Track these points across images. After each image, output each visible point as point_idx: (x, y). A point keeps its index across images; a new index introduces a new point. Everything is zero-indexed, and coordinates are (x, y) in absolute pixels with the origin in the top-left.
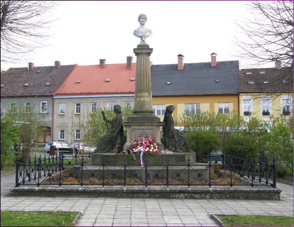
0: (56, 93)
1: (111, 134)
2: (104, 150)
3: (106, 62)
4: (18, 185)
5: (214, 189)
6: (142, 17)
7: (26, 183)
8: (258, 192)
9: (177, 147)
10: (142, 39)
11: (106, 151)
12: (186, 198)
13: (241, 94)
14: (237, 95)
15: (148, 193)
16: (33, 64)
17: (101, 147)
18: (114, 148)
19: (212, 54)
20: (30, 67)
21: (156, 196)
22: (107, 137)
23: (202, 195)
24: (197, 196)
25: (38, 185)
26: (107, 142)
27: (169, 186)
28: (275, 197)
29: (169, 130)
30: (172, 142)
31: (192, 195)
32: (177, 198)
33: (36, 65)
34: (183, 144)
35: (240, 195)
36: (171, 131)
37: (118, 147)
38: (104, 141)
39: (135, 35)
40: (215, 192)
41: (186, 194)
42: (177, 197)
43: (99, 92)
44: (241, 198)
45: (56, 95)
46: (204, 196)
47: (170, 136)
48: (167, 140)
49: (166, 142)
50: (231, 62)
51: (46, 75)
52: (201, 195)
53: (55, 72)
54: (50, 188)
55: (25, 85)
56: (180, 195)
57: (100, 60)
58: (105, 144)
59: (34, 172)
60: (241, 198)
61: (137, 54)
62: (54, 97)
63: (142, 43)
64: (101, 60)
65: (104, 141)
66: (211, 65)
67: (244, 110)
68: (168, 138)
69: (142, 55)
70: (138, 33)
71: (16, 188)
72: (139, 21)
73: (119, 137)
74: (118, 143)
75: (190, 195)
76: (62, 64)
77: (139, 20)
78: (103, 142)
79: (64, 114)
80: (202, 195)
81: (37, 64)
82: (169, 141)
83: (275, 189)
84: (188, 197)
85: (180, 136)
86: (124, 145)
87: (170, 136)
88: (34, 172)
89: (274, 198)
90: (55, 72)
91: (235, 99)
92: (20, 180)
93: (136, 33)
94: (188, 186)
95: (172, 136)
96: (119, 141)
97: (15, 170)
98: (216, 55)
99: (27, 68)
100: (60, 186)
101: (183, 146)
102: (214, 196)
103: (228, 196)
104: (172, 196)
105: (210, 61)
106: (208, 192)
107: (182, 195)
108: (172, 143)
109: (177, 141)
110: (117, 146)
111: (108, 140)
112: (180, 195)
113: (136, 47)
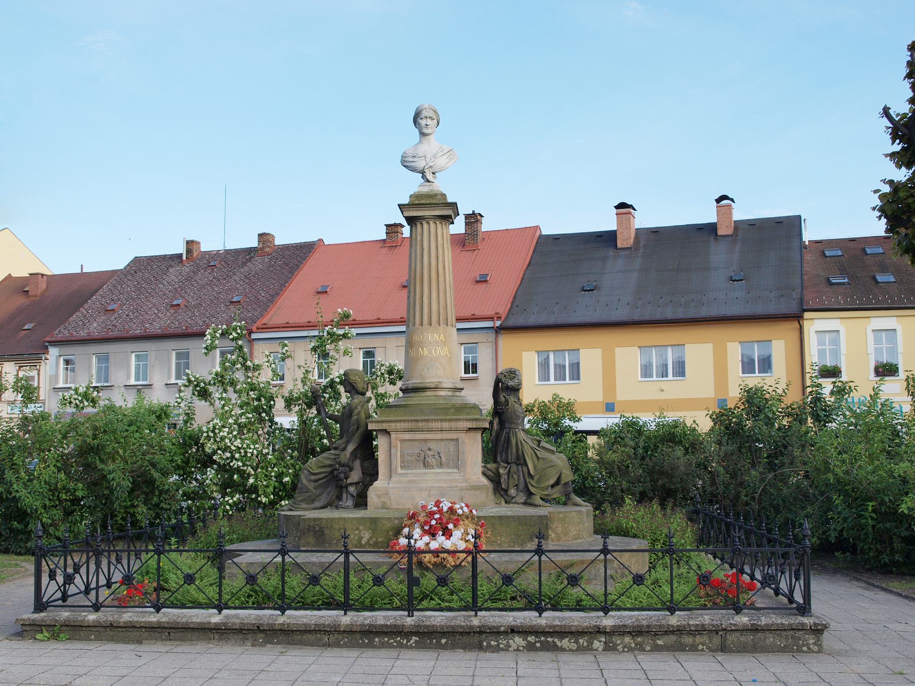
0: (259, 323)
1: (335, 455)
2: (313, 501)
3: (484, 220)
4: (40, 605)
5: (619, 622)
6: (424, 114)
7: (70, 601)
8: (755, 629)
9: (532, 490)
10: (424, 177)
11: (318, 504)
12: (531, 647)
13: (807, 315)
14: (797, 317)
15: (416, 633)
16: (198, 243)
17: (308, 492)
18: (344, 495)
19: (718, 201)
20: (189, 251)
21: (439, 642)
22: (320, 465)
23: (581, 641)
24: (565, 643)
25: (96, 607)
26: (325, 477)
27: (479, 613)
28: (808, 645)
29: (508, 440)
30: (519, 476)
31: (550, 639)
32: (502, 650)
33: (206, 246)
34: (552, 481)
35: (698, 639)
36: (514, 442)
37: (355, 494)
38: (314, 474)
39: (404, 166)
40: (619, 631)
41: (531, 639)
42: (501, 646)
43: (384, 316)
44: (700, 647)
45: (262, 329)
46: (585, 644)
47: (512, 457)
48: (501, 471)
49: (498, 475)
50: (778, 222)
51: (234, 274)
52: (577, 642)
53: (258, 264)
54: (128, 616)
55: (175, 303)
56: (511, 641)
57: (387, 225)
58: (317, 484)
59: (125, 562)
60: (700, 647)
61: (411, 220)
62: (254, 336)
63: (425, 189)
64: (387, 226)
65: (314, 474)
66: (716, 230)
67: (878, 351)
68: (506, 465)
69: (424, 223)
70: (411, 159)
71: (36, 616)
72: (415, 125)
73: (357, 464)
74: (355, 481)
75: (543, 638)
76: (280, 240)
77: (415, 121)
78: (313, 477)
79: (282, 382)
80: (581, 641)
81: (210, 244)
82: (509, 472)
83: (806, 620)
84: (538, 645)
85: (543, 459)
86: (371, 489)
87: (512, 457)
88: (125, 562)
89: (805, 649)
90: (258, 264)
91: (788, 329)
92: (51, 590)
93: (406, 164)
94: (537, 614)
95: (518, 458)
96: (356, 475)
97: (31, 568)
98: (732, 200)
99: (180, 256)
100: (158, 612)
101: (552, 486)
102: (619, 642)
103: (660, 642)
104: (489, 644)
105: (715, 221)
106: (599, 631)
107: (518, 641)
108: (519, 479)
109: (532, 472)
110: (352, 489)
111: (325, 472)
112: (511, 641)
113: (406, 201)
